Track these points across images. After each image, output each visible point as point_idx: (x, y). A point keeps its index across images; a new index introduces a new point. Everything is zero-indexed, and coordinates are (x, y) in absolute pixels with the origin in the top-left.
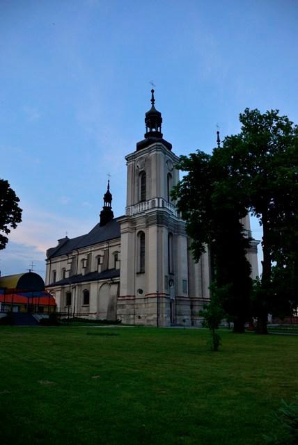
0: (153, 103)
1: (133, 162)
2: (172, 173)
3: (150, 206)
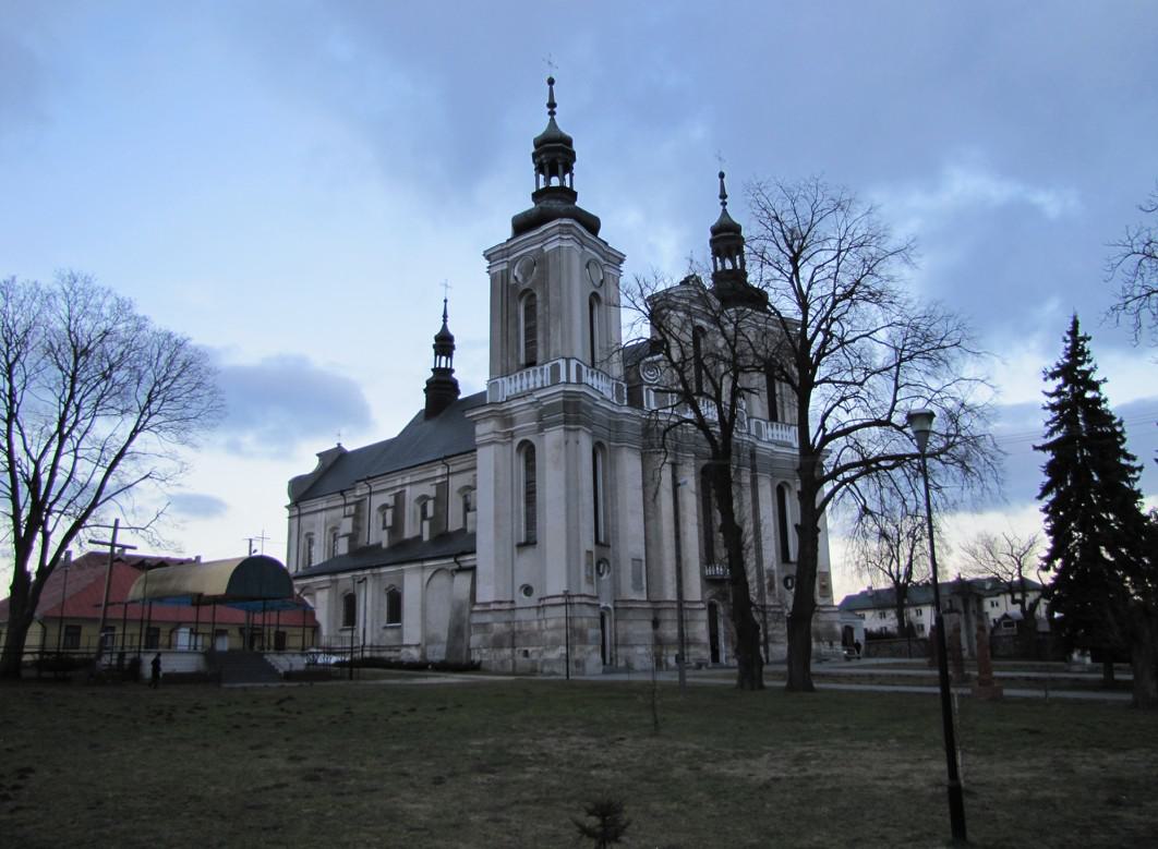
1: (505, 266)
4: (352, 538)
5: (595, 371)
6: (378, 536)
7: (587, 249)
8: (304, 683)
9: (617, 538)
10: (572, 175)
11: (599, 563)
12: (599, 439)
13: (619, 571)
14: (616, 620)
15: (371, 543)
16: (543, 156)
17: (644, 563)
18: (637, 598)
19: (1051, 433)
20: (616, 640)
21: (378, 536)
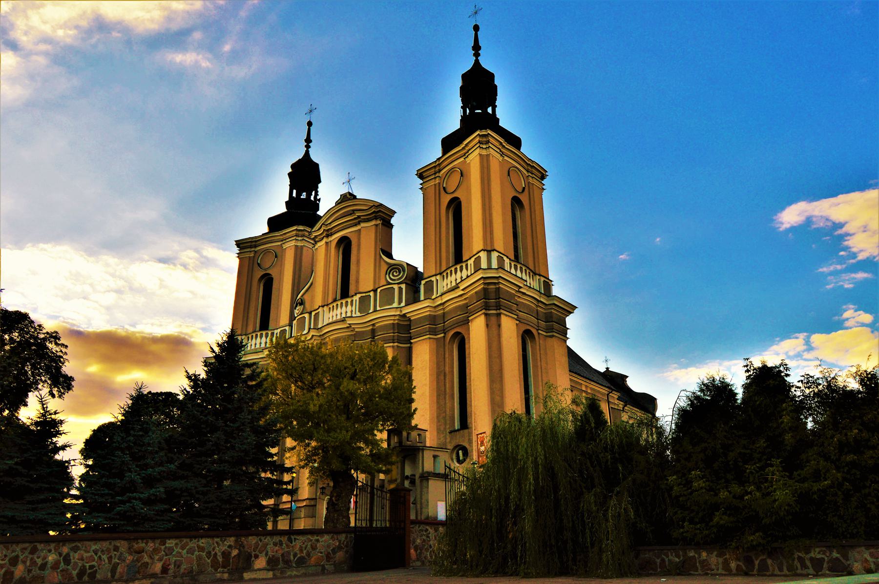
0: (308, 147)
1: (437, 181)
2: (524, 198)
3: (471, 268)
5: (519, 266)
7: (506, 158)
8: (412, 499)
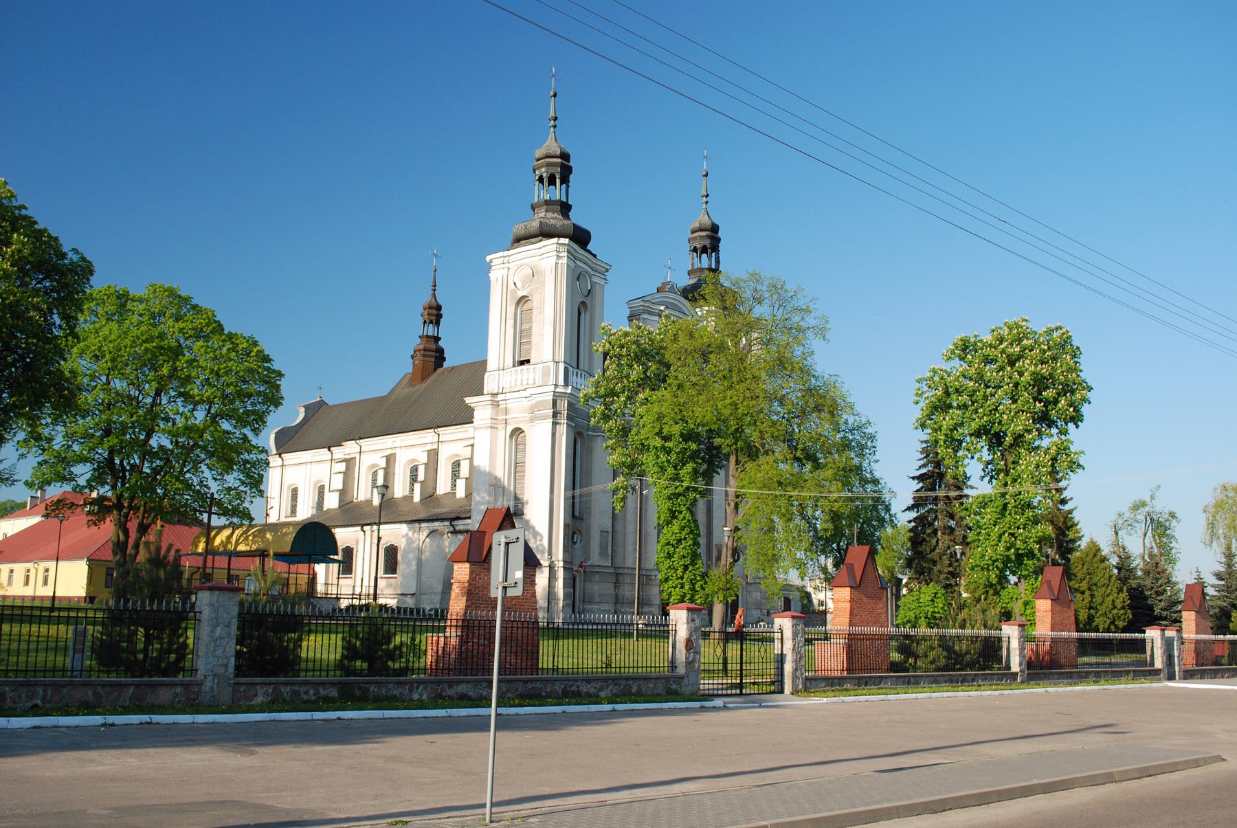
4: (343, 493)
6: (364, 492)
9: (590, 513)
10: (568, 187)
11: (574, 533)
12: (580, 430)
13: (589, 540)
14: (585, 581)
15: (360, 499)
16: (543, 170)
17: (610, 535)
18: (604, 565)
19: (924, 466)
20: (584, 597)
21: (364, 492)
